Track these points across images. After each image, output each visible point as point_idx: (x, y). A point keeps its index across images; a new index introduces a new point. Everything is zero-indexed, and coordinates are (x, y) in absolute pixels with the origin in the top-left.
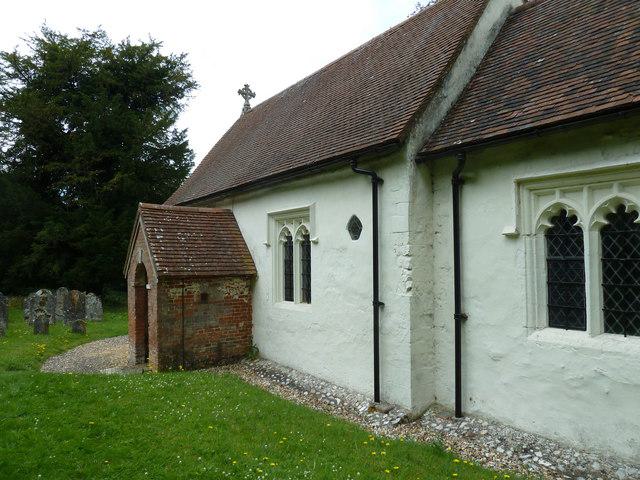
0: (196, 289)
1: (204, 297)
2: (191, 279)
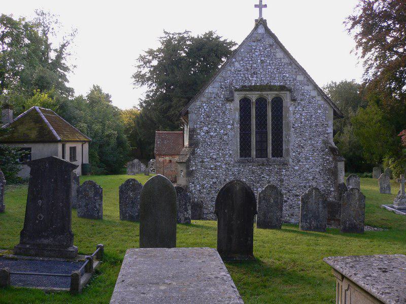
0: (167, 158)
1: (170, 161)
2: (165, 155)
